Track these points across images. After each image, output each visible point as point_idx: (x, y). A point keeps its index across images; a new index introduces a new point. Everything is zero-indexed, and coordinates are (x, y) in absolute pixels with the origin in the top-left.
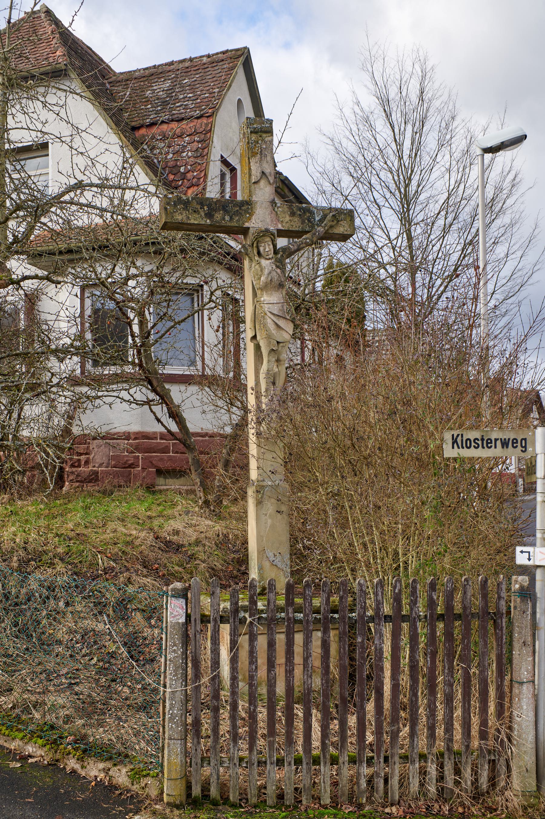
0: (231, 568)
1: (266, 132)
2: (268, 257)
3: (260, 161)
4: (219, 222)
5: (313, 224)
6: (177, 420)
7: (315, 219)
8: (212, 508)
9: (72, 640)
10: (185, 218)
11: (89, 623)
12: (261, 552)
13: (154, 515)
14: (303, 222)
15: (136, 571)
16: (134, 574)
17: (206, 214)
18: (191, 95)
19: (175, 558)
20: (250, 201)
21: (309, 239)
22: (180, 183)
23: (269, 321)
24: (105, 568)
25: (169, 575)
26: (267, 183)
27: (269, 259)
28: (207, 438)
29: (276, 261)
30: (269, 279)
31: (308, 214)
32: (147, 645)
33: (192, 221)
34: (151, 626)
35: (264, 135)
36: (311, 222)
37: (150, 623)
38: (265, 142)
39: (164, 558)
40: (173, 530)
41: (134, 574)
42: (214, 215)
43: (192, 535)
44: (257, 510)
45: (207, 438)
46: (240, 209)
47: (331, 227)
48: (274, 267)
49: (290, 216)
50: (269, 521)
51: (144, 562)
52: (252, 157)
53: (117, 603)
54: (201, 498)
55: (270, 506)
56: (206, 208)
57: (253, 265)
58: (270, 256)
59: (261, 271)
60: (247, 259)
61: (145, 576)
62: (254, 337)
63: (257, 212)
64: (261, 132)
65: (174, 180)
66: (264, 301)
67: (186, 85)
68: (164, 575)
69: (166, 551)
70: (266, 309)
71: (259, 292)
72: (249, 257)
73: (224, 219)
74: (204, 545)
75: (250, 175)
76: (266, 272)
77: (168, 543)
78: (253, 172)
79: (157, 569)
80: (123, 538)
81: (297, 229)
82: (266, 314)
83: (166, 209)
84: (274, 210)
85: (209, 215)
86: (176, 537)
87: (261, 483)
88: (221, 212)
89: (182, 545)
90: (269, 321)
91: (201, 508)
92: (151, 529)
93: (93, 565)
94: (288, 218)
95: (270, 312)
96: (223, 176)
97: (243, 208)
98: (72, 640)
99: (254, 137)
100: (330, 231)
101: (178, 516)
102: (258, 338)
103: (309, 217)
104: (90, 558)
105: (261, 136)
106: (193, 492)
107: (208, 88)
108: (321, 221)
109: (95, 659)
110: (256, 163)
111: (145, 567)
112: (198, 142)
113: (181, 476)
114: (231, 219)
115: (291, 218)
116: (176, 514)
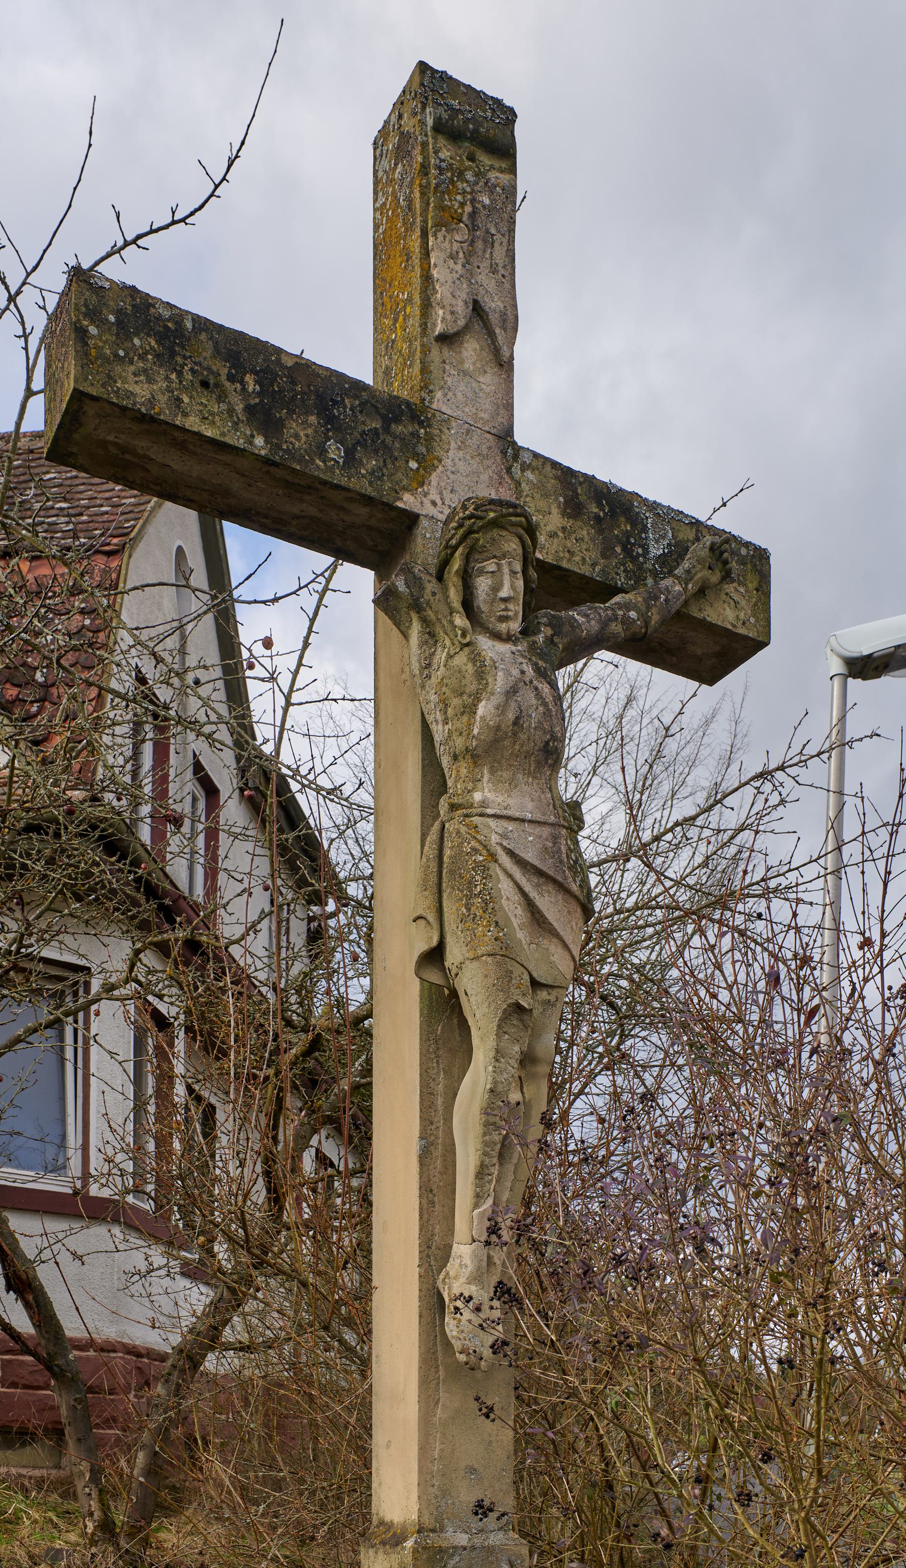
3: (469, 255)
5: (640, 567)
6: (30, 1298)
7: (646, 551)
10: (163, 399)
14: (607, 552)
17: (249, 409)
18: (64, 505)
20: (425, 409)
21: (635, 608)
22: (34, 709)
23: (505, 887)
26: (487, 355)
28: (91, 1353)
30: (511, 716)
33: (193, 423)
35: (485, 160)
36: (634, 559)
38: (491, 189)
45: (91, 1353)
46: (387, 429)
48: (530, 671)
49: (564, 514)
52: (438, 225)
54: (91, 1514)
56: (251, 384)
57: (441, 656)
59: (480, 675)
62: (434, 956)
63: (448, 462)
65: (17, 699)
66: (484, 804)
67: (50, 484)
70: (494, 838)
71: (456, 775)
72: (424, 621)
75: (426, 306)
76: (499, 682)
78: (441, 292)
81: (586, 570)
82: (493, 857)
83: (81, 333)
84: (509, 470)
85: (262, 415)
87: (433, 1540)
88: (313, 419)
90: (505, 887)
91: (93, 1542)
97: (398, 429)
102: (454, 954)
103: (628, 535)
105: (471, 158)
106: (69, 1494)
107: (107, 495)
110: (453, 257)
112: (82, 612)
113: (24, 1444)
114: (351, 459)
115: (569, 523)
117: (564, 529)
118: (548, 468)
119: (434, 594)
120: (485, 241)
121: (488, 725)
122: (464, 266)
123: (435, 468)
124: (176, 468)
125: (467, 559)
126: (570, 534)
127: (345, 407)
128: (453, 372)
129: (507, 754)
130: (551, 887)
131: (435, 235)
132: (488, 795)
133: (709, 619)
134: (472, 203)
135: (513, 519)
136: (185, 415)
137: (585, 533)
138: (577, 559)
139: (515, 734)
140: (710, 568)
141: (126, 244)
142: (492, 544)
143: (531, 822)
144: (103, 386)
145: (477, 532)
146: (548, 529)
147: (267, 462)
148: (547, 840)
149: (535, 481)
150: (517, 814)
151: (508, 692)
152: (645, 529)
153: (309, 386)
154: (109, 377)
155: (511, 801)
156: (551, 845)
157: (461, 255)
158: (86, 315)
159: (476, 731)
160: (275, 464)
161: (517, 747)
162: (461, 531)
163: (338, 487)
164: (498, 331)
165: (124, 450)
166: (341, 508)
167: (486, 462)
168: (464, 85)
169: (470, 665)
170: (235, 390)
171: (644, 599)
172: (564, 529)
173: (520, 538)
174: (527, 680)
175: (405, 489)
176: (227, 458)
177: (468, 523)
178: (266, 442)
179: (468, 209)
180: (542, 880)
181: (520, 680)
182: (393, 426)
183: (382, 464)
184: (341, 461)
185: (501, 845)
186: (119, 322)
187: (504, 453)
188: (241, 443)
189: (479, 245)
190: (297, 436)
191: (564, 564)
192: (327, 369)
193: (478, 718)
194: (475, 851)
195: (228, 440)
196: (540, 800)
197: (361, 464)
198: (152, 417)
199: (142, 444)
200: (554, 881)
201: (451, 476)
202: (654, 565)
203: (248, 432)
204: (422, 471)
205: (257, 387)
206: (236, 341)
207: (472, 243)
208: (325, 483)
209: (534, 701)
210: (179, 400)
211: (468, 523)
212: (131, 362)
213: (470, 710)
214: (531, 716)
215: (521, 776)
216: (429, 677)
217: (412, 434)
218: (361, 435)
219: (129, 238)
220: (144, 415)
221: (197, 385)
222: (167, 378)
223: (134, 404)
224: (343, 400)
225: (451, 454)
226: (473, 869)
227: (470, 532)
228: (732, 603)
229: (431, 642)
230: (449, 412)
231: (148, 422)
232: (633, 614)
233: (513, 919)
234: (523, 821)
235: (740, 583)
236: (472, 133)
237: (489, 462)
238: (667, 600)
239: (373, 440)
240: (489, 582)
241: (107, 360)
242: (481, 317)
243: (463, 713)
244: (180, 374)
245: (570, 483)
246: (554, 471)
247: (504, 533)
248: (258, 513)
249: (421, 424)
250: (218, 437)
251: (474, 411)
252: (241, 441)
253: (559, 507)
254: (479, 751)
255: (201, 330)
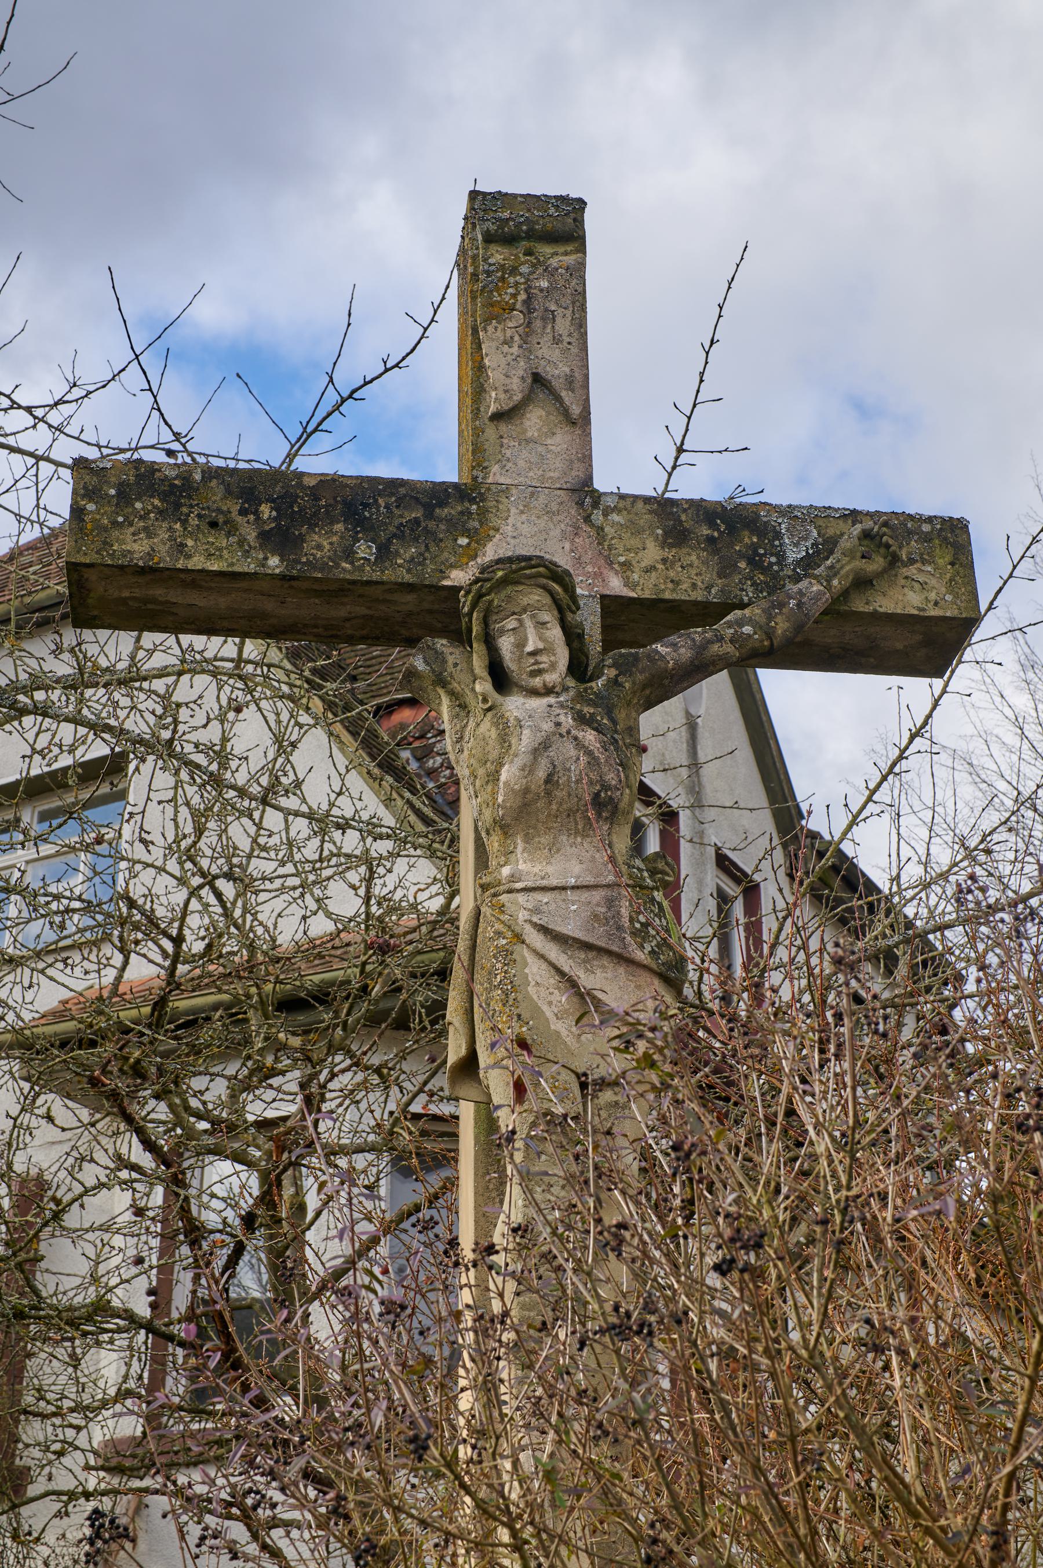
1: (553, 238)
2: (537, 682)
3: (525, 338)
4: (324, 567)
5: (775, 576)
7: (781, 557)
10: (163, 550)
17: (264, 537)
21: (750, 621)
23: (535, 970)
27: (548, 691)
29: (580, 697)
30: (541, 774)
31: (749, 539)
33: (197, 562)
35: (545, 249)
36: (766, 570)
38: (550, 272)
42: (302, 539)
46: (429, 515)
47: (862, 583)
48: (567, 721)
49: (664, 544)
52: (487, 320)
56: (266, 511)
58: (552, 678)
59: (504, 739)
60: (445, 702)
64: (532, 235)
66: (513, 878)
70: (522, 915)
72: (453, 694)
73: (349, 554)
76: (525, 741)
78: (494, 376)
81: (698, 595)
84: (587, 519)
85: (281, 538)
88: (339, 527)
90: (535, 970)
94: (652, 553)
95: (544, 930)
96: (723, 899)
99: (498, 255)
100: (859, 605)
103: (754, 547)
105: (529, 253)
108: (808, 563)
114: (384, 552)
117: (664, 561)
118: (640, 505)
119: (456, 665)
120: (544, 319)
121: (512, 790)
122: (520, 347)
123: (490, 538)
124: (201, 604)
125: (485, 622)
126: (673, 563)
127: (379, 506)
128: (512, 443)
129: (542, 817)
130: (605, 961)
131: (485, 329)
132: (522, 866)
133: (881, 610)
134: (526, 290)
135: (528, 572)
136: (189, 557)
137: (694, 558)
138: (684, 586)
139: (548, 793)
140: (863, 557)
141: (343, 401)
142: (508, 602)
143: (573, 888)
144: (97, 553)
145: (488, 594)
146: (643, 564)
147: (283, 577)
148: (598, 905)
149: (622, 522)
150: (554, 882)
151: (536, 750)
152: (778, 535)
153: (335, 498)
154: (105, 543)
155: (550, 869)
156: (603, 910)
157: (517, 338)
158: (83, 496)
159: (500, 799)
160: (293, 578)
161: (554, 807)
162: (470, 597)
163: (369, 583)
164: (563, 394)
165: (146, 601)
166: (385, 601)
167: (556, 519)
168: (522, 196)
169: (493, 729)
170: (248, 522)
171: (763, 611)
172: (664, 561)
173: (545, 588)
174: (563, 731)
175: (453, 566)
176: (244, 584)
177: (475, 587)
178: (282, 561)
179: (523, 296)
180: (591, 955)
181: (554, 734)
182: (437, 510)
183: (423, 548)
184: (373, 558)
185: (530, 921)
186: (120, 494)
187: (580, 504)
188: (252, 568)
189: (538, 324)
190: (319, 547)
191: (667, 596)
192: (357, 477)
193: (501, 785)
194: (499, 934)
195: (237, 569)
196: (593, 859)
197: (397, 554)
198: (151, 568)
199: (158, 592)
200: (609, 953)
201: (512, 541)
202: (794, 570)
203: (261, 556)
204: (474, 545)
205: (274, 513)
206: (251, 478)
207: (529, 324)
208: (354, 582)
209: (573, 753)
210: (183, 545)
211: (475, 587)
212: (131, 524)
213: (493, 777)
214: (569, 770)
215: (564, 838)
216: (461, 751)
217: (462, 513)
218: (398, 528)
219: (345, 394)
220: (142, 568)
221: (205, 528)
222: (170, 529)
223: (132, 560)
224: (376, 501)
225: (510, 521)
226: (494, 956)
227: (480, 596)
228: (917, 586)
229: (462, 714)
230: (509, 481)
231: (149, 572)
232: (747, 629)
233: (545, 1008)
234: (564, 888)
235: (924, 562)
236: (527, 232)
237: (561, 517)
238: (799, 605)
239: (412, 530)
240: (512, 639)
241: (105, 529)
242: (543, 385)
243: (487, 782)
244: (184, 523)
245: (672, 513)
246: (648, 507)
247: (520, 588)
248: (305, 626)
249: (473, 500)
250: (225, 569)
251: (540, 472)
252: (252, 566)
253: (656, 539)
254: (508, 820)
255: (211, 479)
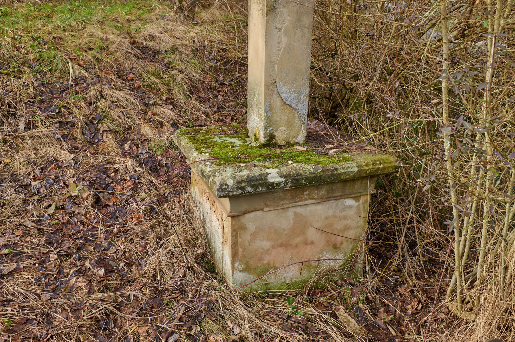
0: (209, 78)
8: (186, 14)
9: (29, 174)
11: (50, 151)
12: (271, 86)
13: (134, 18)
15: (109, 83)
16: (107, 87)
19: (152, 67)
24: (76, 78)
25: (144, 86)
32: (119, 182)
34: (125, 154)
37: (124, 149)
39: (139, 66)
40: (150, 35)
41: (107, 87)
43: (168, 42)
44: (267, 22)
50: (284, 40)
51: (118, 72)
53: (86, 123)
54: (175, 3)
55: (286, 16)
61: (119, 89)
68: (139, 87)
69: (142, 58)
74: (181, 53)
77: (144, 49)
79: (132, 80)
80: (99, 42)
86: (152, 43)
89: (159, 51)
92: (128, 33)
93: (65, 72)
98: (29, 174)
101: (154, 19)
104: (61, 65)
109: (53, 207)
111: (119, 77)
116: (154, 18)
